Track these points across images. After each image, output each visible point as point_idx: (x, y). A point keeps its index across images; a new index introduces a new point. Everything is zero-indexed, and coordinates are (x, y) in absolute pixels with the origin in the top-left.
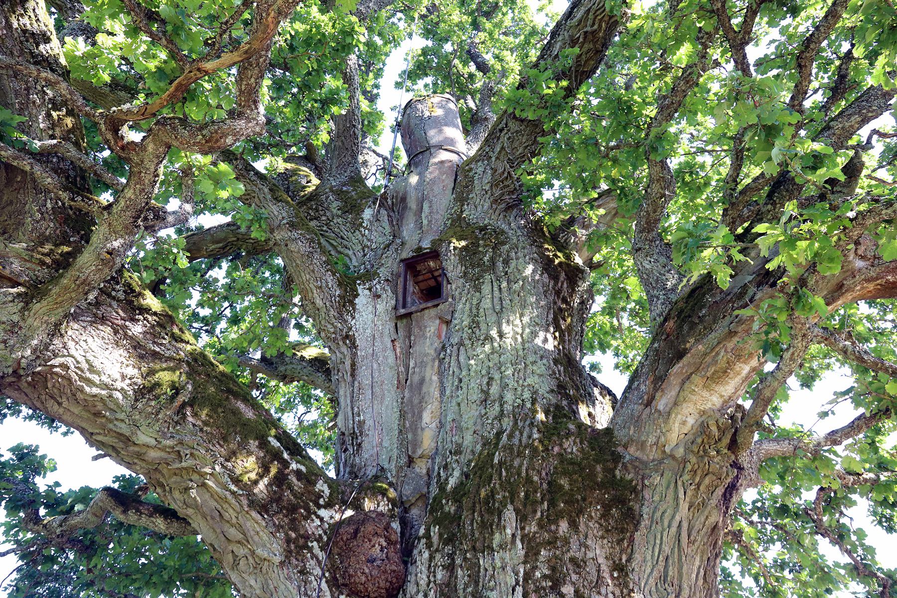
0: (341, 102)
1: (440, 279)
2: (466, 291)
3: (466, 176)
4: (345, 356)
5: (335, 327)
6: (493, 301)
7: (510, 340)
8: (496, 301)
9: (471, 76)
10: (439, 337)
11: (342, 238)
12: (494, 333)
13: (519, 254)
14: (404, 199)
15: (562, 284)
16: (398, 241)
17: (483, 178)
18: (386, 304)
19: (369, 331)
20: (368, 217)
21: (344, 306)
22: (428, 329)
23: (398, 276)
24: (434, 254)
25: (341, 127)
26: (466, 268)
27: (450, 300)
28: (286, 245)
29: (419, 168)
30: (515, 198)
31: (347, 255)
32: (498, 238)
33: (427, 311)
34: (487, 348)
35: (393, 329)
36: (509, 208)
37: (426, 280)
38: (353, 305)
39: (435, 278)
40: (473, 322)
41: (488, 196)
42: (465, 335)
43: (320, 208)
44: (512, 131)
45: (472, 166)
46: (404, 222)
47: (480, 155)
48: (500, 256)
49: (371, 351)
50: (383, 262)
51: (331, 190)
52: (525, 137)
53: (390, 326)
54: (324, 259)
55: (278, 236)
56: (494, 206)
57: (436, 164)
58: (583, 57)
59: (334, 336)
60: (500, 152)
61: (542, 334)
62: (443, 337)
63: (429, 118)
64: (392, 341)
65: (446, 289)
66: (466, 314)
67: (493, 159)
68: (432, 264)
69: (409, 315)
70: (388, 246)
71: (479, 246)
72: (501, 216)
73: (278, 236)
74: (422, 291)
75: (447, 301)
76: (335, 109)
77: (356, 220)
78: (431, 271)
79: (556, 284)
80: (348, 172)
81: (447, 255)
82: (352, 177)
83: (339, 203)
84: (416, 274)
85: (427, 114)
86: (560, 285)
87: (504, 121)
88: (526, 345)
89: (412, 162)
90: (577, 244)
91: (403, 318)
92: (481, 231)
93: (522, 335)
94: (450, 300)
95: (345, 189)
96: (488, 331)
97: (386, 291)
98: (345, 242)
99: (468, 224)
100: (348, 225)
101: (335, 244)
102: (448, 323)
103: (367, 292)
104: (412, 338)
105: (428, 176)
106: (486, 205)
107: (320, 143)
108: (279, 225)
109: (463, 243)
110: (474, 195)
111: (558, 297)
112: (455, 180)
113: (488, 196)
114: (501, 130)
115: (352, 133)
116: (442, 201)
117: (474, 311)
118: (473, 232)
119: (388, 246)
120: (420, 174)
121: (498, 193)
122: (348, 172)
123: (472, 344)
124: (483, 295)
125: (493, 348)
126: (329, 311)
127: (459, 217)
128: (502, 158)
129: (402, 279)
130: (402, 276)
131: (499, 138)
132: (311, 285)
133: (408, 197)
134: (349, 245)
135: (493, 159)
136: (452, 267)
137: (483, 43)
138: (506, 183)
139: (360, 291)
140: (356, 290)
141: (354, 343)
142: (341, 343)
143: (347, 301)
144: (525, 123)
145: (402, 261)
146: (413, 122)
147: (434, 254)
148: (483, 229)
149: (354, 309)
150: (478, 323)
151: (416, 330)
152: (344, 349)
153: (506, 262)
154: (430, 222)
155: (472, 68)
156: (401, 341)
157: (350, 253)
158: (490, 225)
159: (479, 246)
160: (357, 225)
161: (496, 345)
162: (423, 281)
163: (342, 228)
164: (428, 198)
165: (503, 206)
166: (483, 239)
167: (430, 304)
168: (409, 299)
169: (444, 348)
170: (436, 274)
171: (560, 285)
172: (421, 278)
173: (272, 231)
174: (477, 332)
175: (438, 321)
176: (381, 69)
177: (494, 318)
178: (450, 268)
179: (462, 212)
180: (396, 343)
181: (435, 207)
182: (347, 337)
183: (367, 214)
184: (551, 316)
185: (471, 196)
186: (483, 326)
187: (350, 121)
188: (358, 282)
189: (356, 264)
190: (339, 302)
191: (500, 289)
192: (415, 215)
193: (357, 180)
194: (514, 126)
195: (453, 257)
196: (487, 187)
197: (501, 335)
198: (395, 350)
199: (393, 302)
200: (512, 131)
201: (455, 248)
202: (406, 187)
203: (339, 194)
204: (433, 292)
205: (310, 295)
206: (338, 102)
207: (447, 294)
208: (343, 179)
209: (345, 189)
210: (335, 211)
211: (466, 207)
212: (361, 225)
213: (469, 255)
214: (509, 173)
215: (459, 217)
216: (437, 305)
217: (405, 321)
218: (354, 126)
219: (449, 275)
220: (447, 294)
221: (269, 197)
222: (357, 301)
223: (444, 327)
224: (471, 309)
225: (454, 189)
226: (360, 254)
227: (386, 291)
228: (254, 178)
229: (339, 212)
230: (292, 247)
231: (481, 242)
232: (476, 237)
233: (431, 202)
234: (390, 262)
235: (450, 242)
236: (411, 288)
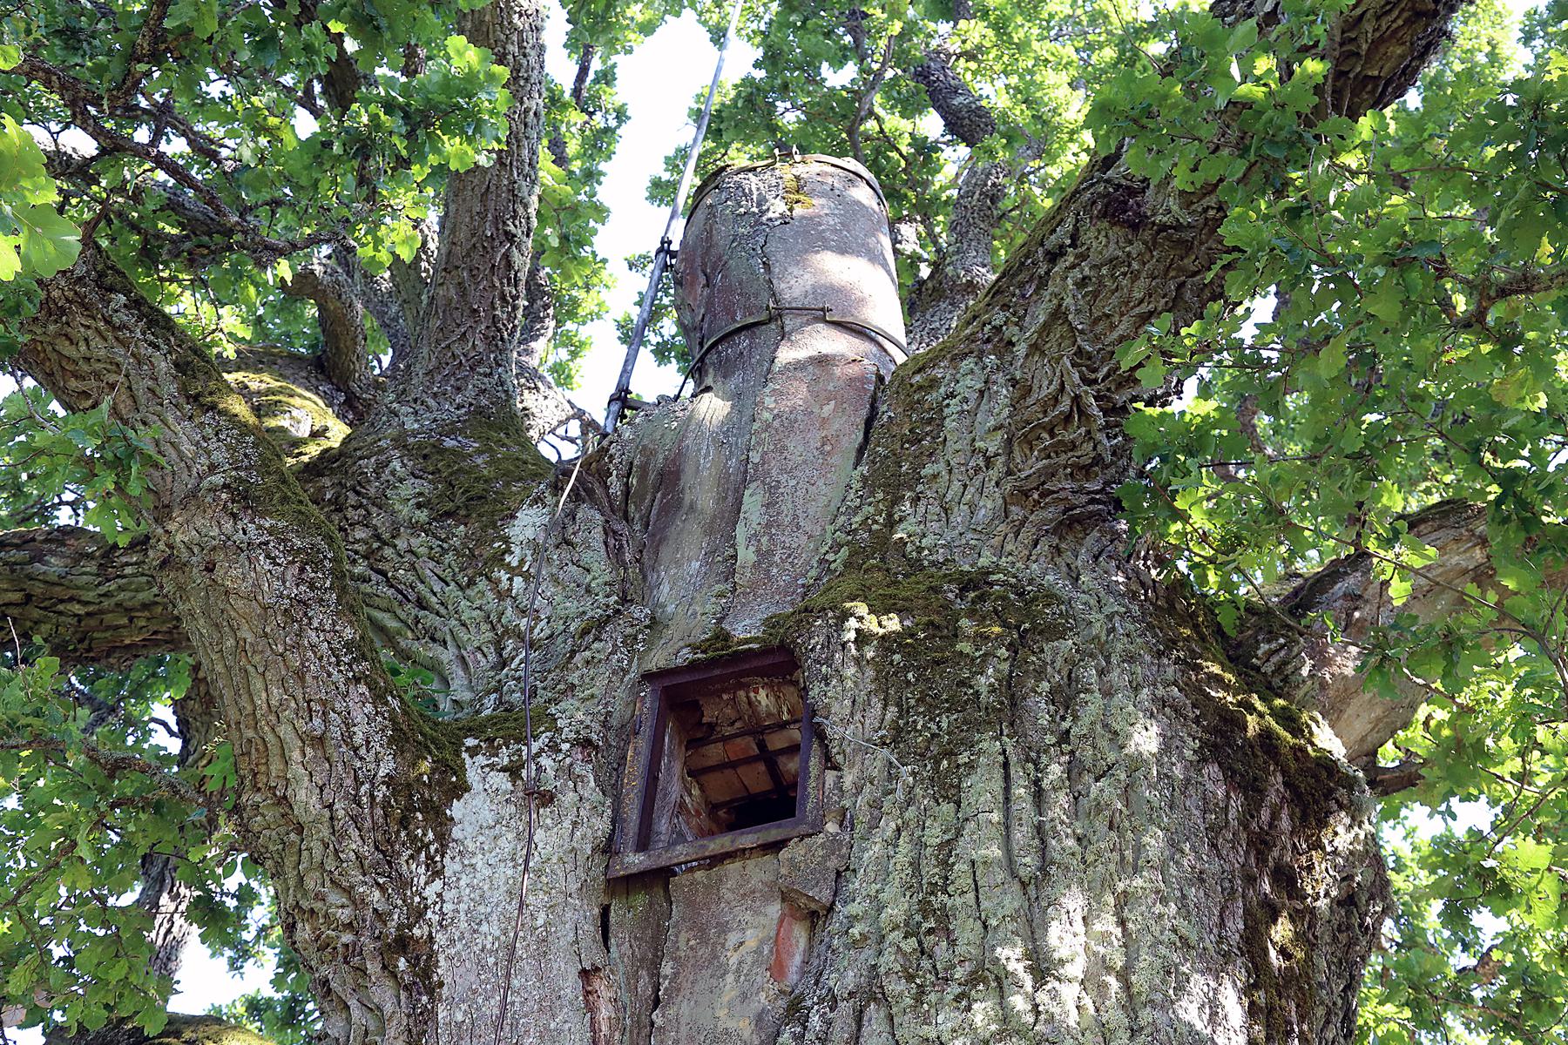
0: (479, 126)
1: (791, 765)
2: (900, 795)
3: (911, 407)
4: (382, 1022)
5: (358, 903)
6: (1007, 838)
7: (1075, 988)
8: (1021, 835)
9: (925, 150)
10: (777, 970)
11: (421, 604)
12: (1012, 957)
13: (1114, 676)
14: (670, 478)
15: (1275, 816)
16: (637, 612)
17: (977, 410)
18: (572, 828)
19: (491, 929)
20: (530, 533)
21: (404, 822)
22: (733, 938)
23: (629, 730)
24: (779, 660)
25: (462, 235)
26: (903, 712)
27: (831, 827)
28: (210, 568)
29: (735, 380)
30: (1093, 477)
31: (434, 667)
32: (1029, 620)
33: (733, 867)
34: (982, 1013)
35: (590, 929)
36: (1071, 524)
37: (733, 765)
38: (441, 824)
39: (769, 758)
40: (925, 909)
41: (994, 474)
42: (889, 960)
43: (352, 499)
44: (1094, 258)
45: (938, 373)
46: (665, 553)
47: (971, 339)
48: (1040, 674)
49: (492, 1008)
50: (574, 678)
51: (400, 442)
52: (1142, 283)
53: (580, 916)
54: (348, 633)
55: (181, 531)
56: (1016, 512)
57: (799, 366)
58: (1368, 26)
59: (347, 938)
60: (1046, 328)
61: (1199, 984)
62: (793, 976)
63: (785, 221)
64: (585, 974)
65: (819, 785)
66: (896, 879)
67: (1021, 349)
68: (763, 698)
69: (661, 876)
70: (602, 623)
71: (956, 635)
72: (1044, 547)
73: (181, 531)
74: (713, 808)
75: (818, 829)
76: (453, 148)
77: (480, 542)
78: (758, 729)
79: (1251, 810)
80: (470, 391)
81: (829, 662)
82: (481, 411)
83: (424, 486)
84: (697, 736)
85: (778, 208)
86: (1265, 815)
87: (1069, 225)
88: (1146, 1016)
89: (713, 357)
90: (1323, 685)
91: (635, 887)
92: (964, 589)
93: (1124, 976)
94: (831, 827)
95: (449, 443)
96: (986, 948)
97: (577, 779)
98: (430, 620)
99: (916, 566)
100: (449, 558)
101: (392, 624)
102: (816, 917)
103: (501, 781)
104: (667, 969)
105: (769, 402)
106: (987, 507)
107: (384, 257)
108: (193, 494)
109: (893, 624)
110: (941, 467)
111: (1261, 860)
112: (869, 423)
113: (994, 474)
114: (1054, 257)
115: (496, 274)
116: (818, 489)
117: (931, 871)
118: (935, 590)
119: (602, 623)
120: (737, 397)
121: (1032, 465)
122: (470, 391)
123: (919, 998)
124: (966, 810)
125: (1006, 1017)
126: (342, 836)
127: (881, 542)
128: (1051, 347)
129: (642, 743)
130: (646, 731)
131: (1043, 283)
132: (285, 731)
133: (689, 470)
134: (443, 628)
135: (1021, 349)
136: (847, 700)
137: (970, 56)
138: (1068, 436)
139: (472, 776)
140: (460, 770)
141: (427, 973)
142: (373, 967)
143: (417, 813)
144: (1147, 235)
145: (648, 677)
146: (722, 232)
147: (779, 660)
148: (975, 583)
149: (443, 839)
150: (944, 916)
151: (682, 940)
152: (384, 994)
153: (1065, 698)
154: (764, 556)
155: (931, 125)
156: (619, 977)
157: (447, 655)
158: (998, 569)
159: (956, 635)
160: (482, 561)
161: (1019, 1002)
162: (724, 754)
163: (427, 568)
164: (761, 473)
165: (1051, 513)
166: (971, 614)
167: (748, 839)
168: (663, 825)
169: (795, 1010)
170: (777, 742)
171: (1265, 815)
172: (714, 753)
173: (162, 513)
174: (941, 951)
175: (775, 909)
176: (607, 131)
177: (1012, 901)
178: (841, 708)
179: (891, 524)
180: (598, 984)
181: (787, 508)
182: (402, 944)
183: (527, 524)
184: (1236, 925)
185: (928, 470)
186: (967, 932)
187: (499, 220)
188: (470, 742)
189: (467, 696)
190: (386, 805)
191: (1039, 796)
192: (709, 531)
193: (505, 423)
194: (1102, 240)
195: (850, 671)
196: (993, 445)
197: (1042, 968)
198: (591, 1008)
199: (602, 825)
200: (1094, 258)
201: (862, 638)
202: (681, 433)
203: (426, 455)
204: (763, 801)
205: (276, 766)
206: (469, 124)
207: (822, 806)
208: (449, 411)
209: (449, 443)
210: (405, 511)
211: (907, 506)
212: (498, 559)
213: (918, 669)
214: (1076, 399)
215: (881, 542)
216: (775, 847)
217: (640, 900)
218: (510, 237)
219: (834, 731)
220: (822, 806)
221: (170, 389)
222: (457, 809)
223: (799, 935)
224: (915, 865)
225: (861, 451)
226: (485, 662)
227: (577, 779)
228: (122, 317)
229: (422, 516)
230: (232, 574)
231: (964, 622)
232: (947, 605)
233: (772, 489)
234: (601, 682)
235: (846, 615)
236: (674, 784)
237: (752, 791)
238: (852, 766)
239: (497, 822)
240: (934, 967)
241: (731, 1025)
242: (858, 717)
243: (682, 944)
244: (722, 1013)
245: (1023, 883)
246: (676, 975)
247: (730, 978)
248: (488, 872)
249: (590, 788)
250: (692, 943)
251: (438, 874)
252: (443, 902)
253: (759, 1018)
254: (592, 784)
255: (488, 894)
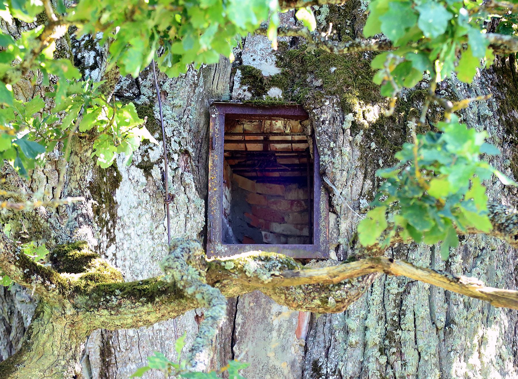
195: (347, 149)
237: (249, 150)
238: (346, 218)
239: (139, 204)
240: (394, 374)
241: (277, 364)
242: (349, 183)
243: (246, 304)
244: (271, 355)
245: (437, 328)
246: (244, 323)
247: (275, 334)
248: (137, 240)
249: (193, 193)
250: (252, 305)
251: (112, 240)
252: (116, 259)
253: (293, 365)
254: (194, 190)
255: (139, 256)
